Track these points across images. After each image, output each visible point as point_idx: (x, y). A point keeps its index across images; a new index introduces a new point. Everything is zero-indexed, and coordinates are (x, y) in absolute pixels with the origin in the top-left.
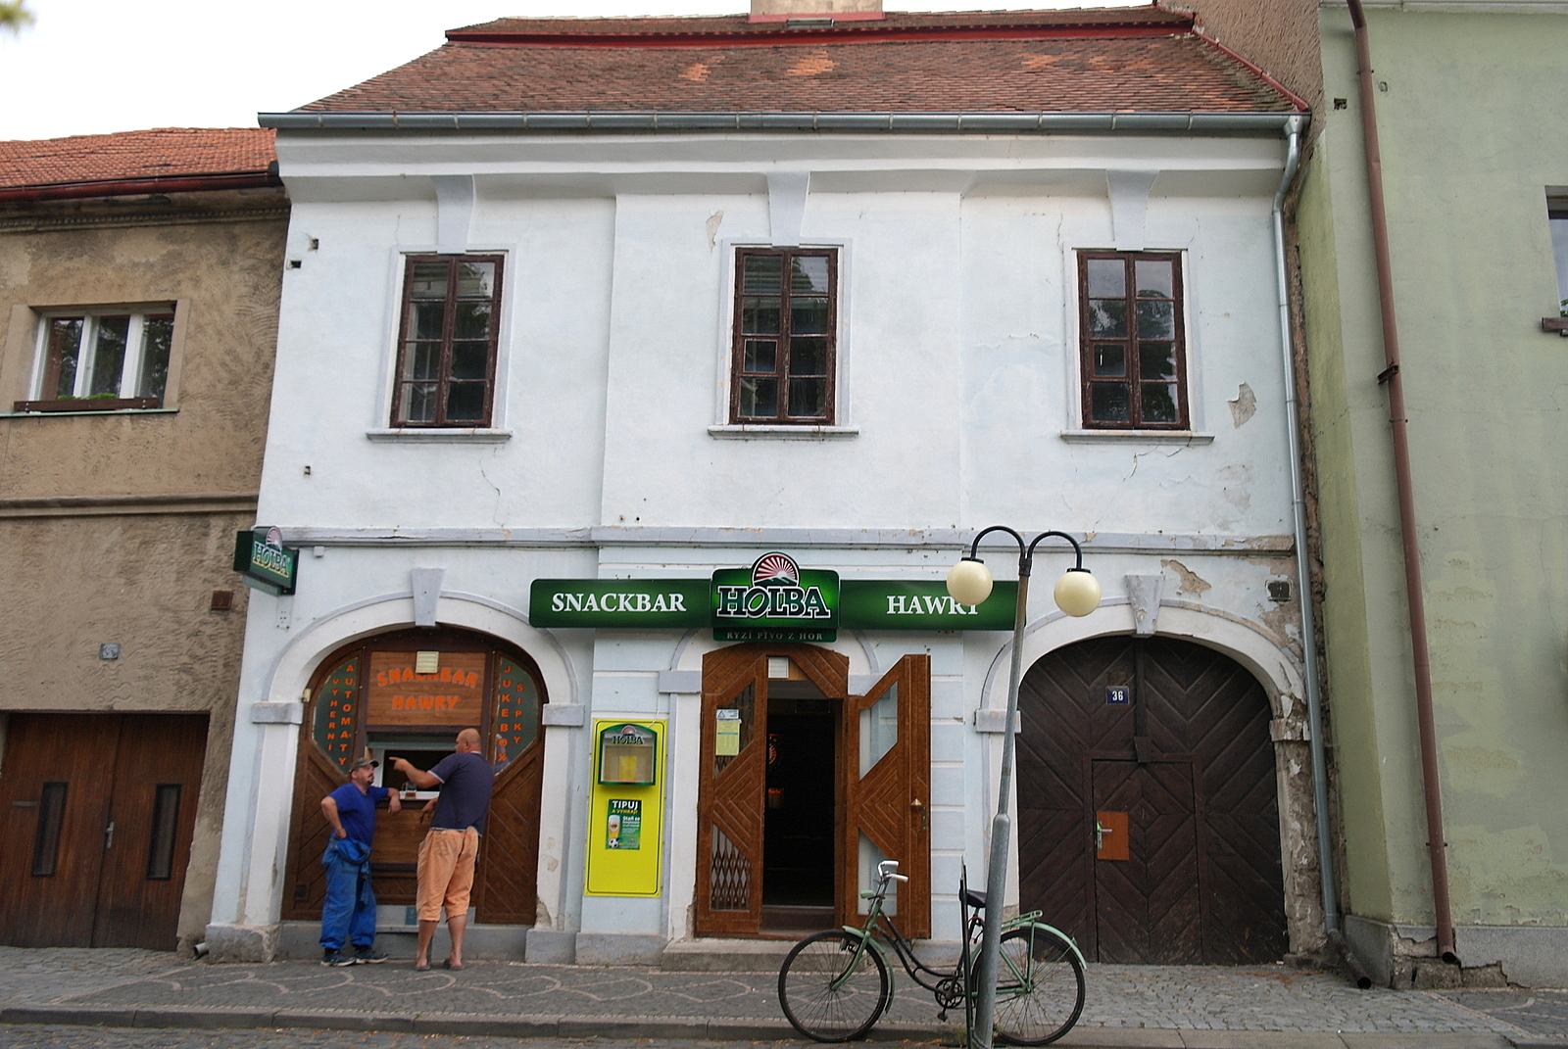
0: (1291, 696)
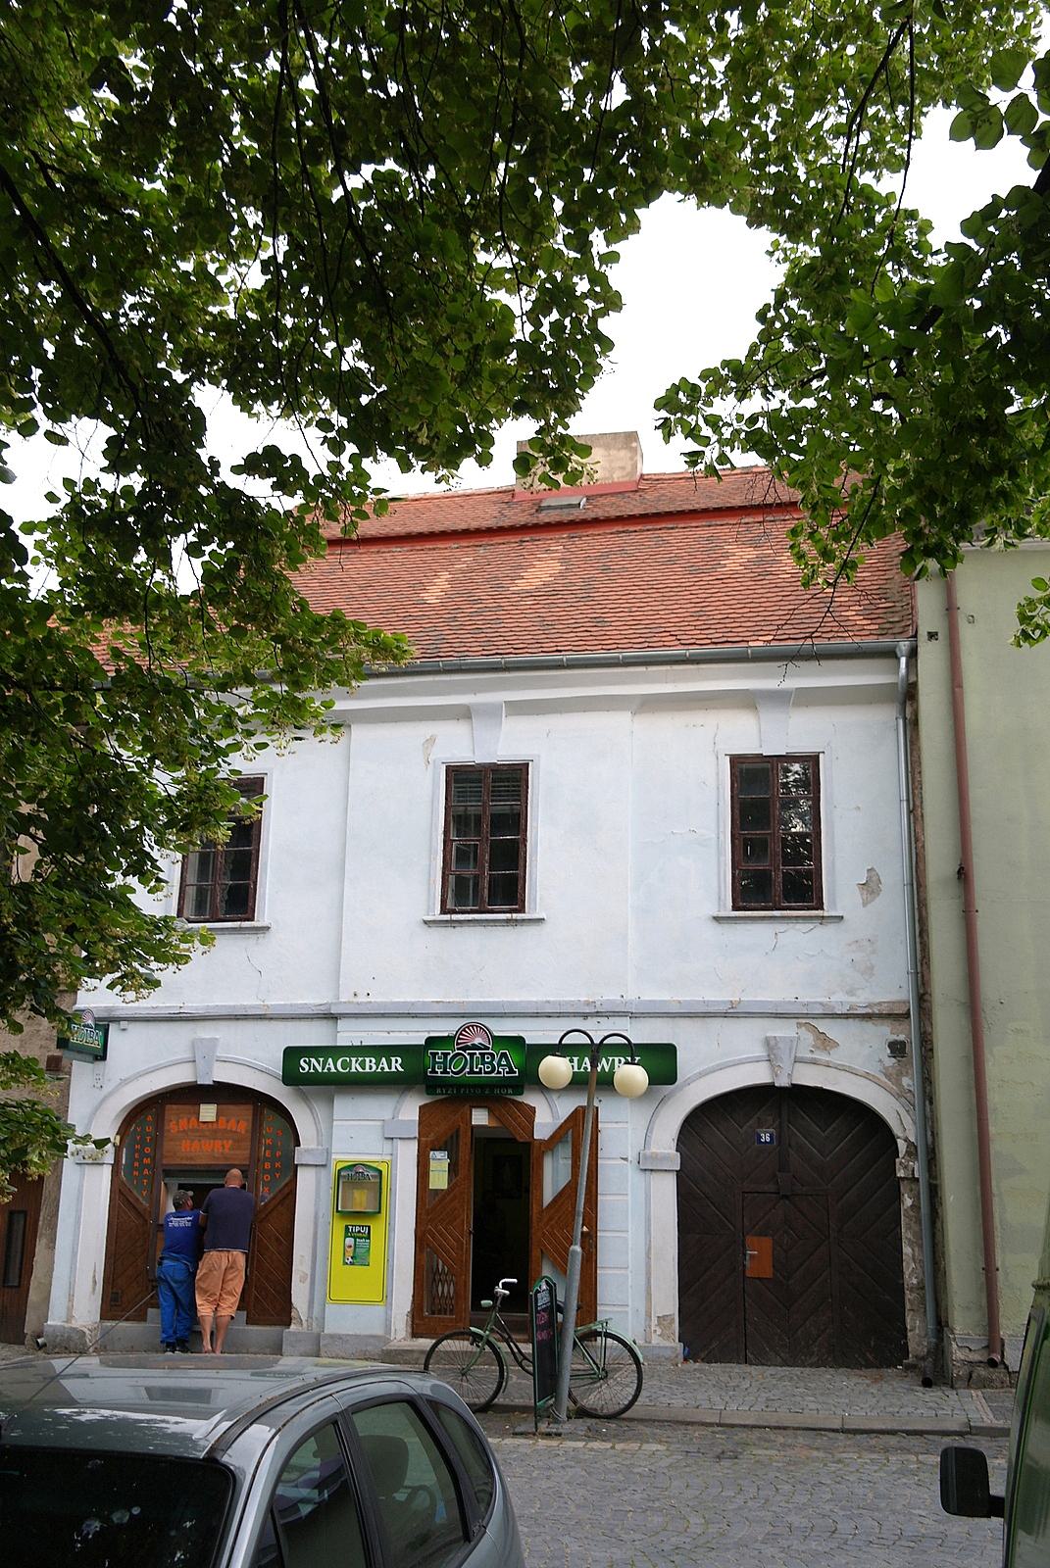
0: (906, 1140)
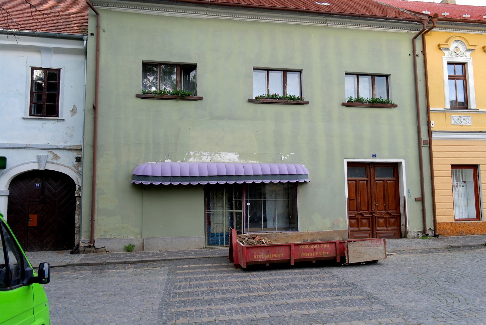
0: (79, 185)
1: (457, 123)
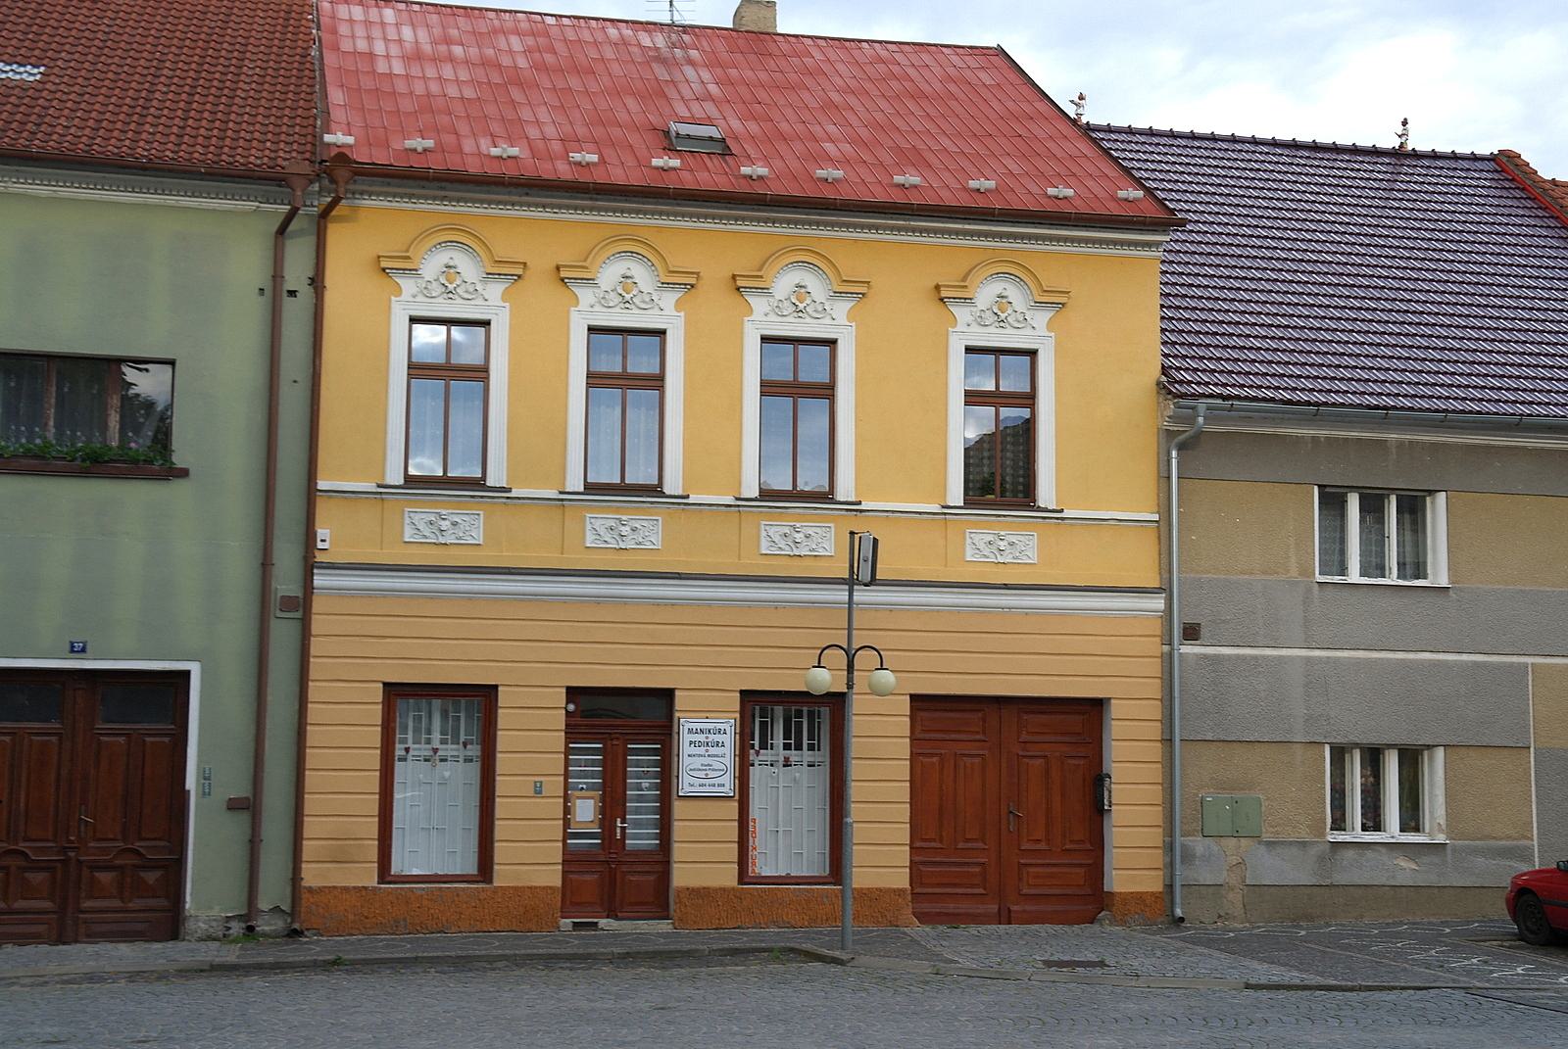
1: (425, 537)
